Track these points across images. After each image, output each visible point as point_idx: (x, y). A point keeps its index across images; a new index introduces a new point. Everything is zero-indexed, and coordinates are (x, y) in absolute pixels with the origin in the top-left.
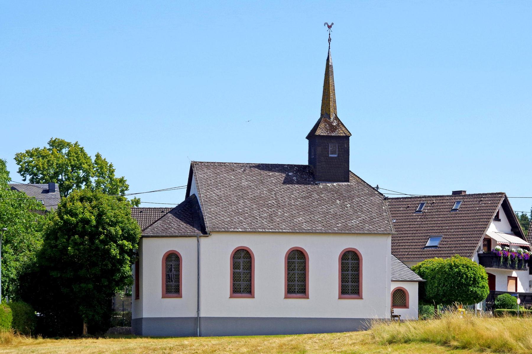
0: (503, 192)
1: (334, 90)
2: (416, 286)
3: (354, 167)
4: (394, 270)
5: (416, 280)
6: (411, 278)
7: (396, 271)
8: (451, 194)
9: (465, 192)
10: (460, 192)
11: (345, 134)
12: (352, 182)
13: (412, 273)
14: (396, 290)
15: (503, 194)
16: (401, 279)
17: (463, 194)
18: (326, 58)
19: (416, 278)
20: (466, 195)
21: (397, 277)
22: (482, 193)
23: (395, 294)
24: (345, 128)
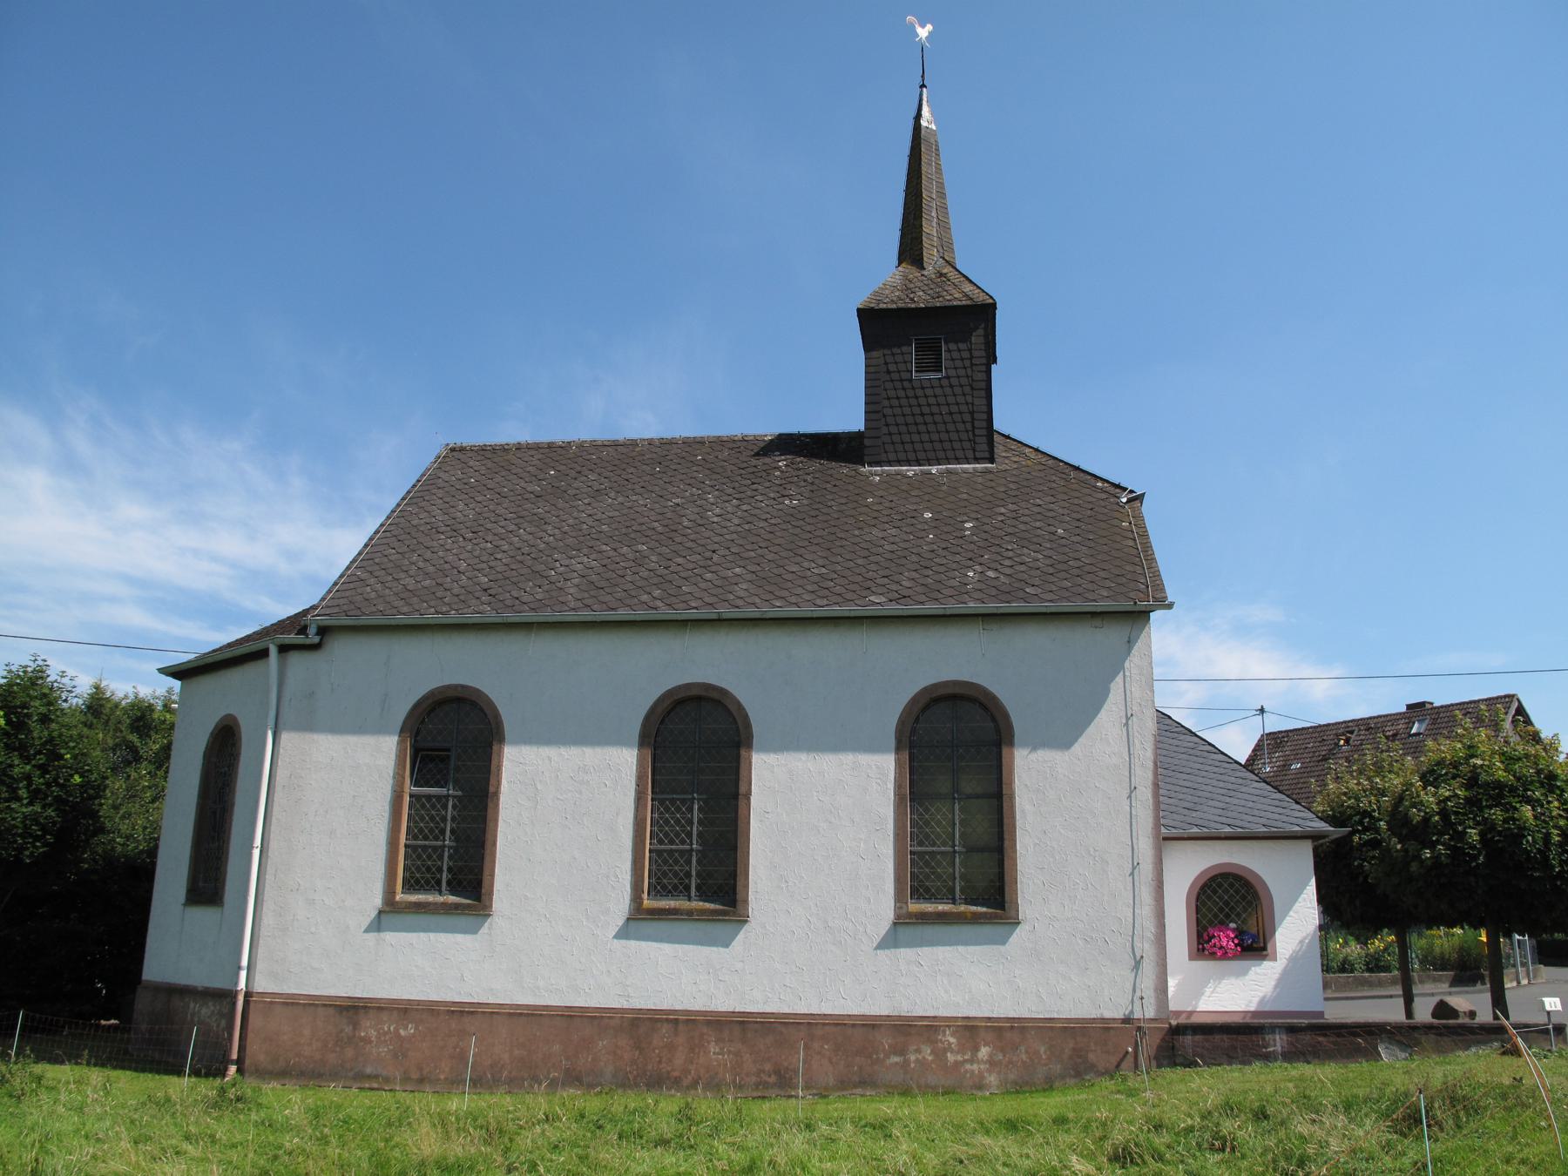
0: (1512, 693)
1: (942, 195)
2: (1303, 856)
3: (1005, 419)
4: (1200, 793)
5: (1297, 828)
6: (1275, 824)
7: (1209, 795)
8: (1404, 709)
9: (1432, 704)
10: (1422, 704)
11: (971, 299)
12: (1005, 460)
13: (1277, 803)
14: (1213, 879)
15: (1513, 696)
16: (1228, 829)
17: (1428, 706)
18: (913, 113)
19: (1300, 822)
20: (1436, 708)
21: (1211, 817)
22: (1467, 700)
23: (1204, 903)
24: (1101, 479)
